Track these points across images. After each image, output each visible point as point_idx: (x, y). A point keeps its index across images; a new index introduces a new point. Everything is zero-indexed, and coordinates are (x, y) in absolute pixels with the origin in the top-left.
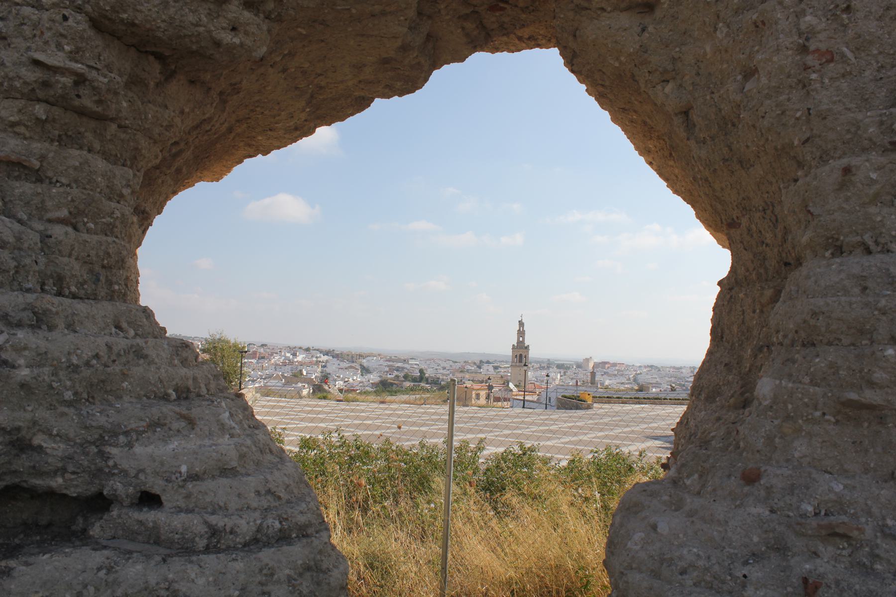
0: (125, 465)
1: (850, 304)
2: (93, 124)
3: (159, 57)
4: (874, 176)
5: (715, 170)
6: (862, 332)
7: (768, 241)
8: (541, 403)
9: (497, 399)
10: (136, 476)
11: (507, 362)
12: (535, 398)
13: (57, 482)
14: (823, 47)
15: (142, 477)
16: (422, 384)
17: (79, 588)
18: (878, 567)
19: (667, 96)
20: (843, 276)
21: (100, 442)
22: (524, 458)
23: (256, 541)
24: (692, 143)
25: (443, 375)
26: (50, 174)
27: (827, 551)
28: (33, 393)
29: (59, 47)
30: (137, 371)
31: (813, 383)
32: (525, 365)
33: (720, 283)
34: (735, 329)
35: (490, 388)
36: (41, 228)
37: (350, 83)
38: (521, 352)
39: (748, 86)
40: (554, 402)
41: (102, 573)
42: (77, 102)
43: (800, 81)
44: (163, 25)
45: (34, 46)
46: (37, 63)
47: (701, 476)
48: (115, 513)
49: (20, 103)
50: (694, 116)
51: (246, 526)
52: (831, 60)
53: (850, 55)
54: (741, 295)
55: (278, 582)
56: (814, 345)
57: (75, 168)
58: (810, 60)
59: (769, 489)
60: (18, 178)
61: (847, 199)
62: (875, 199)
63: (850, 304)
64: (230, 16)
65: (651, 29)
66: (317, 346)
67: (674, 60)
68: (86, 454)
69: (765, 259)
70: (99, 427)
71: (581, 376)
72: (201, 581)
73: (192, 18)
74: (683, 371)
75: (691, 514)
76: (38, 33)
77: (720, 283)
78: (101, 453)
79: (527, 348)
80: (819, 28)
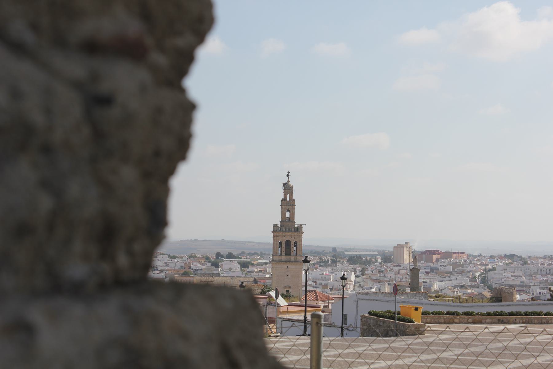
11: (262, 255)
38: (288, 236)
79: (299, 229)
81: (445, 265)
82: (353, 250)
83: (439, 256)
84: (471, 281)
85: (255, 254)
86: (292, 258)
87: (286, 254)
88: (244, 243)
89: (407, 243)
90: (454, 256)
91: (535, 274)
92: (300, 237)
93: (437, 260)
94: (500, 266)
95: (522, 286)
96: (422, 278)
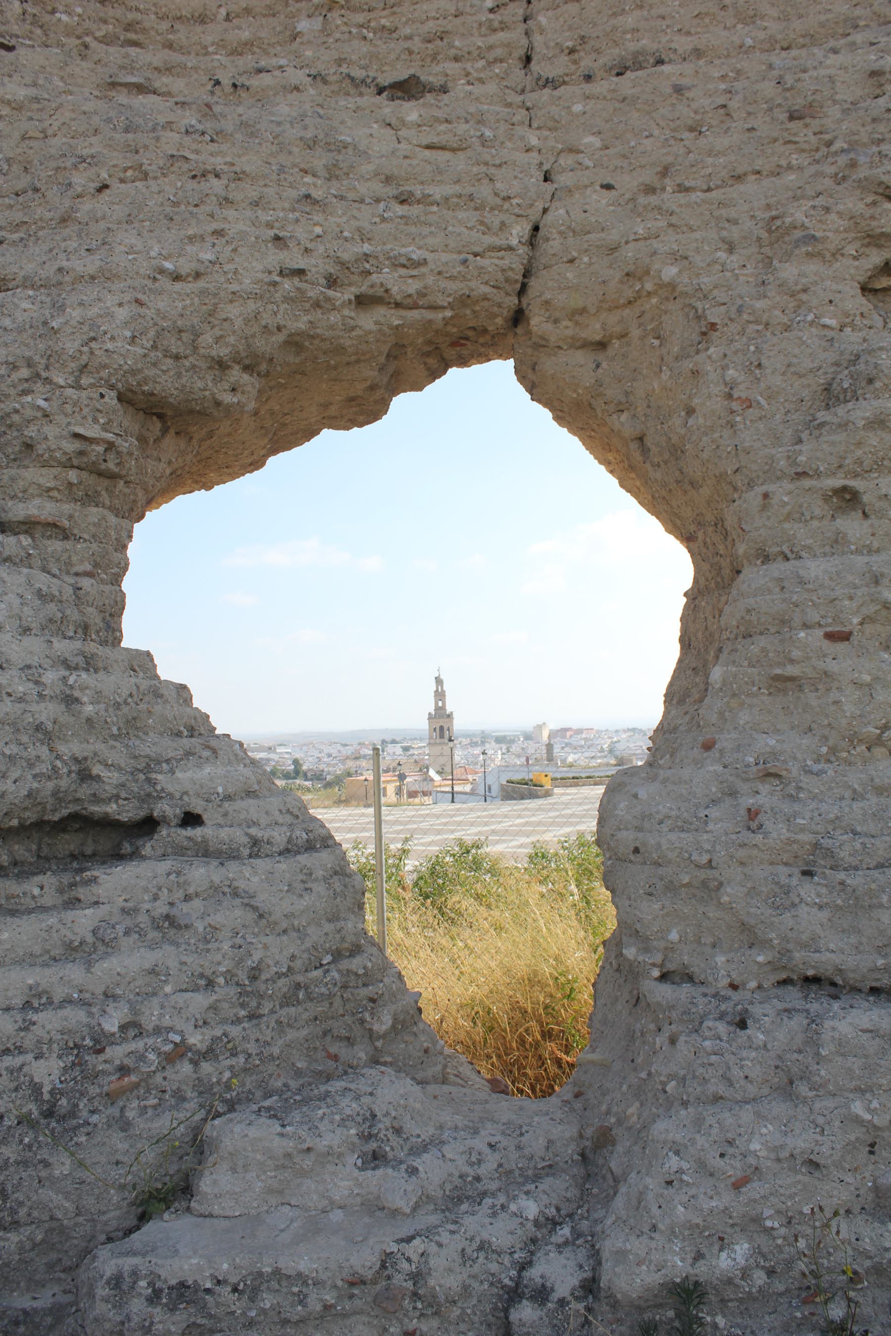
0: (170, 789)
1: (773, 601)
2: (106, 482)
3: (161, 416)
4: (786, 499)
5: (670, 490)
6: (783, 622)
7: (721, 552)
8: (477, 795)
9: (412, 794)
10: (181, 799)
11: (421, 740)
12: (468, 788)
13: (111, 808)
14: (743, 395)
15: (185, 798)
16: (298, 781)
17: (155, 890)
18: (801, 795)
19: (623, 425)
20: (767, 579)
21: (148, 769)
22: (469, 857)
23: (288, 851)
24: (648, 466)
25: (328, 765)
26: (75, 531)
27: (764, 788)
28: (94, 728)
29: (95, 420)
30: (158, 709)
31: (751, 665)
32: (450, 740)
33: (686, 594)
34: (700, 635)
35: (402, 777)
36: (72, 581)
37: (314, 420)
38: (442, 722)
39: (691, 422)
40: (495, 790)
41: (173, 877)
42: (103, 466)
43: (728, 422)
44: (175, 393)
45: (73, 421)
46: (77, 436)
47: (671, 756)
48: (164, 832)
49: (55, 471)
50: (648, 442)
51: (279, 837)
52: (750, 406)
53: (763, 402)
54: (703, 604)
55: (316, 880)
56: (751, 636)
57: (94, 525)
58: (735, 405)
59: (722, 751)
60: (50, 537)
61: (769, 518)
62: (788, 517)
63: (773, 601)
64: (232, 379)
65: (604, 365)
67: (627, 394)
68: (137, 781)
69: (720, 568)
70: (147, 756)
71: (531, 751)
72: (255, 879)
73: (200, 384)
75: (665, 781)
76: (77, 409)
77: (686, 594)
78: (148, 780)
79: (450, 716)
80: (739, 380)
81: (577, 740)
85: (415, 739)
92: (452, 722)
96: (556, 750)
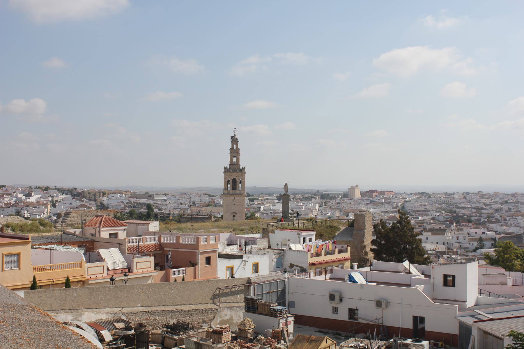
38: (234, 176)
66: (59, 186)
74: (455, 196)
79: (242, 171)
82: (332, 191)
83: (377, 194)
84: (393, 208)
86: (238, 192)
87: (233, 189)
88: (263, 188)
89: (357, 186)
90: (386, 193)
91: (435, 203)
93: (376, 196)
94: (414, 199)
95: (425, 211)
